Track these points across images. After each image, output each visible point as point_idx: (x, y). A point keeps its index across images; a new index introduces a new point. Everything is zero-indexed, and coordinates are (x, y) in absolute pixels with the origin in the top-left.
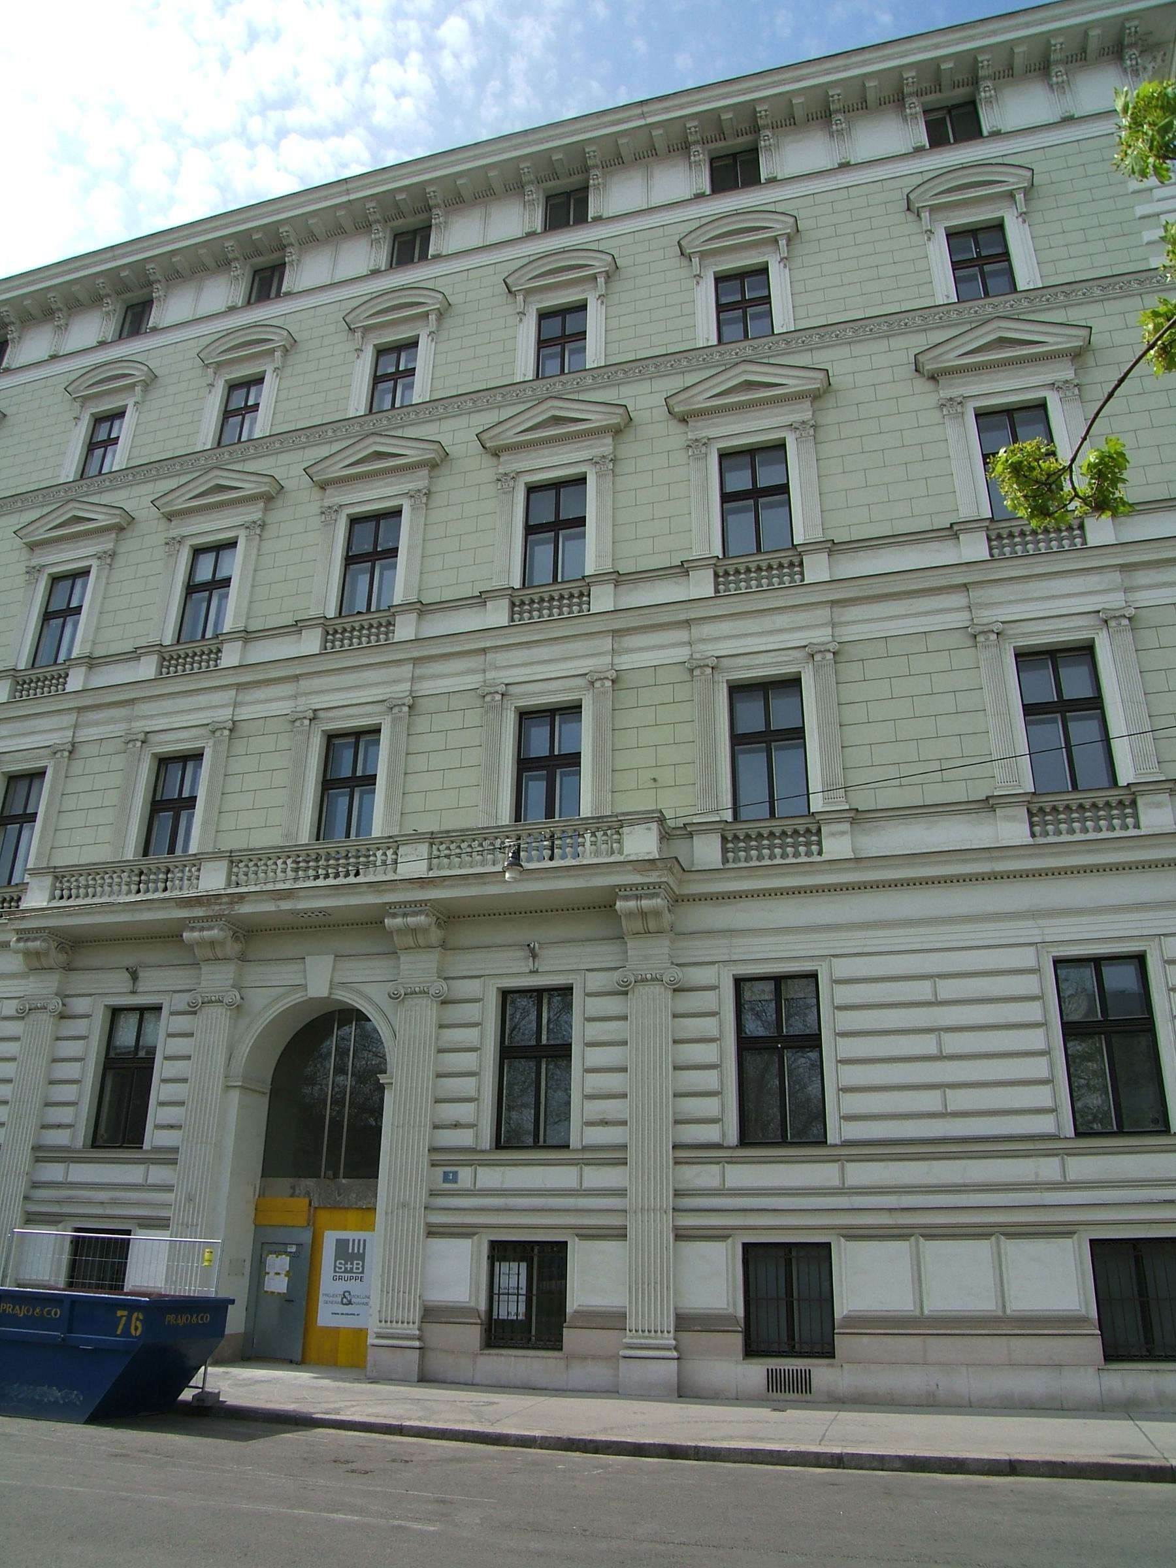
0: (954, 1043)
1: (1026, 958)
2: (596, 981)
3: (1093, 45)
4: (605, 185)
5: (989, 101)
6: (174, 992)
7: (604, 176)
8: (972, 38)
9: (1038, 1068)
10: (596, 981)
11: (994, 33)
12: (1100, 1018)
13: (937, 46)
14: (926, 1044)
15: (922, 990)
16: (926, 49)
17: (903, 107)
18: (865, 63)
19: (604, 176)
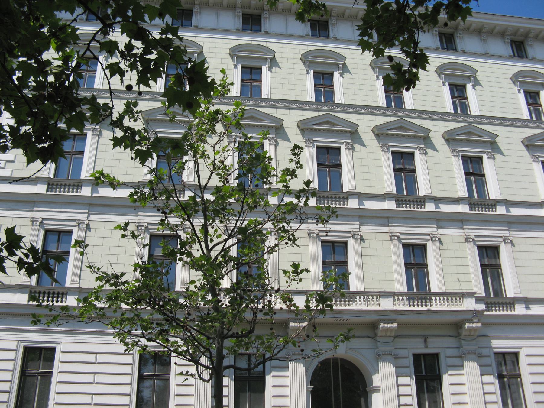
0: (89, 378)
1: (13, 345)
2: (450, 352)
3: (496, 31)
4: (200, 12)
5: (266, 18)
6: (446, 348)
7: (200, 8)
8: (530, 24)
9: (126, 390)
10: (450, 352)
11: (537, 24)
12: (424, 373)
13: (520, 23)
14: (99, 379)
15: (91, 358)
16: (517, 22)
17: (236, 10)
18: (498, 20)
19: (200, 8)
